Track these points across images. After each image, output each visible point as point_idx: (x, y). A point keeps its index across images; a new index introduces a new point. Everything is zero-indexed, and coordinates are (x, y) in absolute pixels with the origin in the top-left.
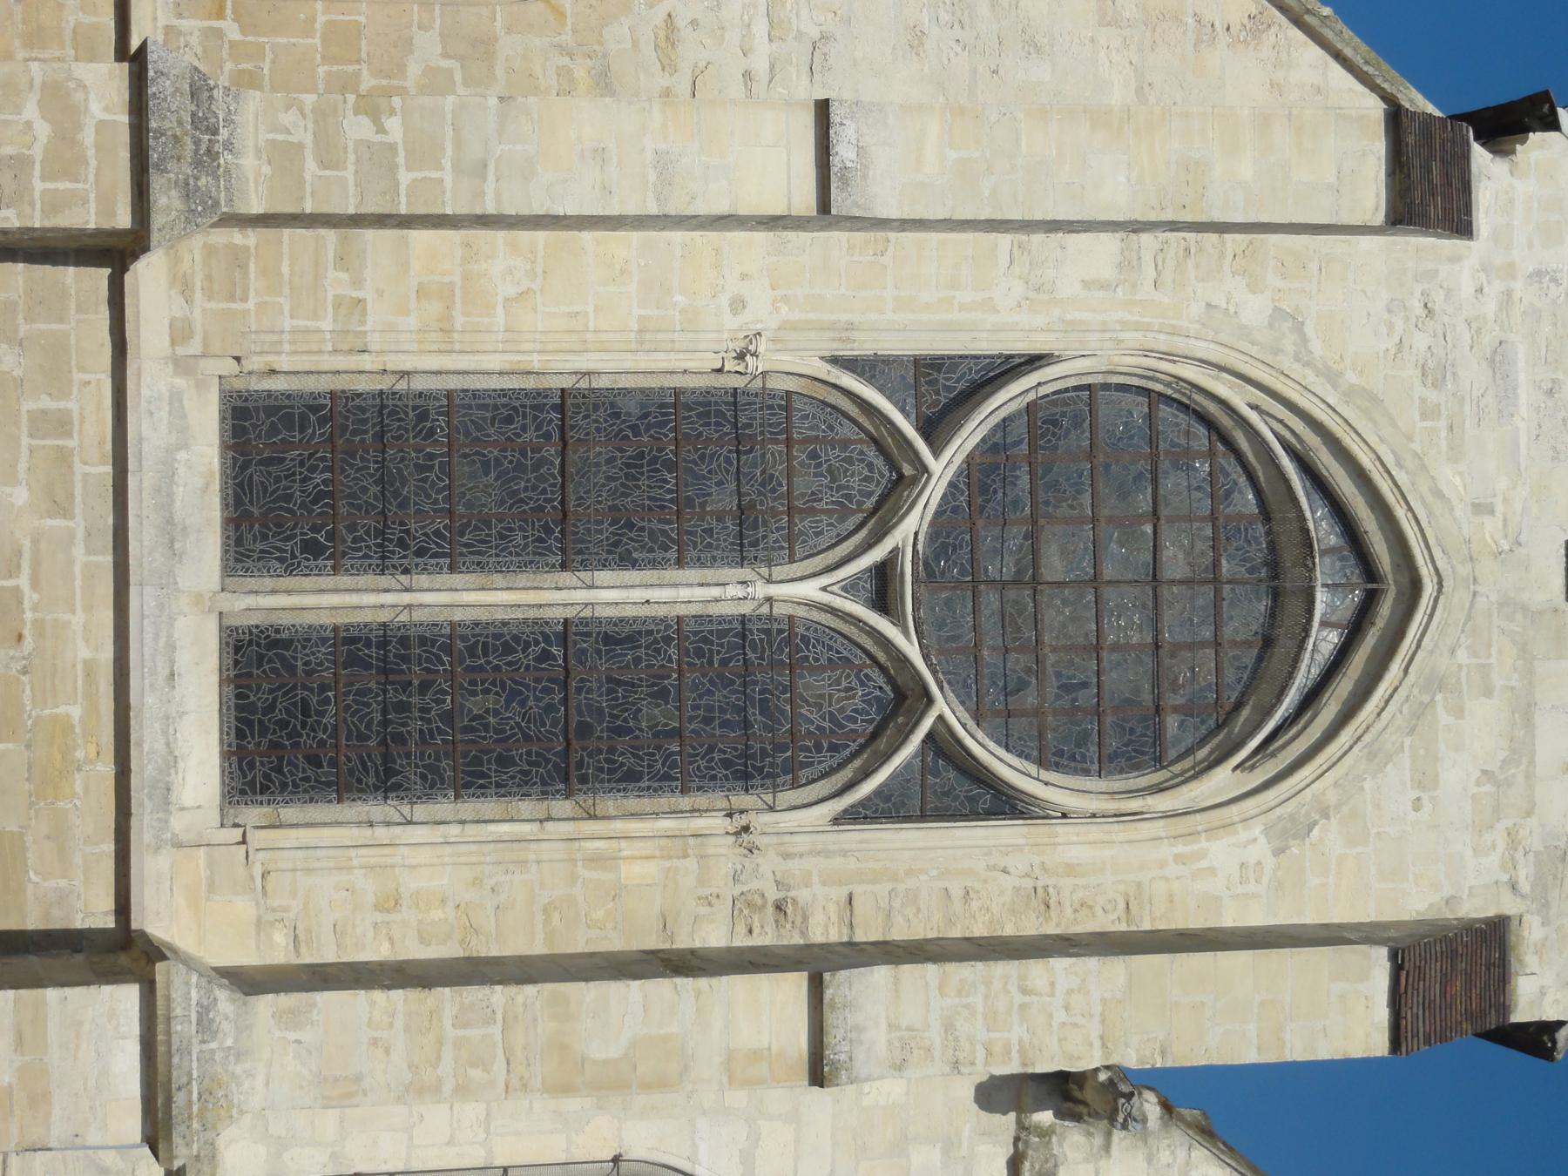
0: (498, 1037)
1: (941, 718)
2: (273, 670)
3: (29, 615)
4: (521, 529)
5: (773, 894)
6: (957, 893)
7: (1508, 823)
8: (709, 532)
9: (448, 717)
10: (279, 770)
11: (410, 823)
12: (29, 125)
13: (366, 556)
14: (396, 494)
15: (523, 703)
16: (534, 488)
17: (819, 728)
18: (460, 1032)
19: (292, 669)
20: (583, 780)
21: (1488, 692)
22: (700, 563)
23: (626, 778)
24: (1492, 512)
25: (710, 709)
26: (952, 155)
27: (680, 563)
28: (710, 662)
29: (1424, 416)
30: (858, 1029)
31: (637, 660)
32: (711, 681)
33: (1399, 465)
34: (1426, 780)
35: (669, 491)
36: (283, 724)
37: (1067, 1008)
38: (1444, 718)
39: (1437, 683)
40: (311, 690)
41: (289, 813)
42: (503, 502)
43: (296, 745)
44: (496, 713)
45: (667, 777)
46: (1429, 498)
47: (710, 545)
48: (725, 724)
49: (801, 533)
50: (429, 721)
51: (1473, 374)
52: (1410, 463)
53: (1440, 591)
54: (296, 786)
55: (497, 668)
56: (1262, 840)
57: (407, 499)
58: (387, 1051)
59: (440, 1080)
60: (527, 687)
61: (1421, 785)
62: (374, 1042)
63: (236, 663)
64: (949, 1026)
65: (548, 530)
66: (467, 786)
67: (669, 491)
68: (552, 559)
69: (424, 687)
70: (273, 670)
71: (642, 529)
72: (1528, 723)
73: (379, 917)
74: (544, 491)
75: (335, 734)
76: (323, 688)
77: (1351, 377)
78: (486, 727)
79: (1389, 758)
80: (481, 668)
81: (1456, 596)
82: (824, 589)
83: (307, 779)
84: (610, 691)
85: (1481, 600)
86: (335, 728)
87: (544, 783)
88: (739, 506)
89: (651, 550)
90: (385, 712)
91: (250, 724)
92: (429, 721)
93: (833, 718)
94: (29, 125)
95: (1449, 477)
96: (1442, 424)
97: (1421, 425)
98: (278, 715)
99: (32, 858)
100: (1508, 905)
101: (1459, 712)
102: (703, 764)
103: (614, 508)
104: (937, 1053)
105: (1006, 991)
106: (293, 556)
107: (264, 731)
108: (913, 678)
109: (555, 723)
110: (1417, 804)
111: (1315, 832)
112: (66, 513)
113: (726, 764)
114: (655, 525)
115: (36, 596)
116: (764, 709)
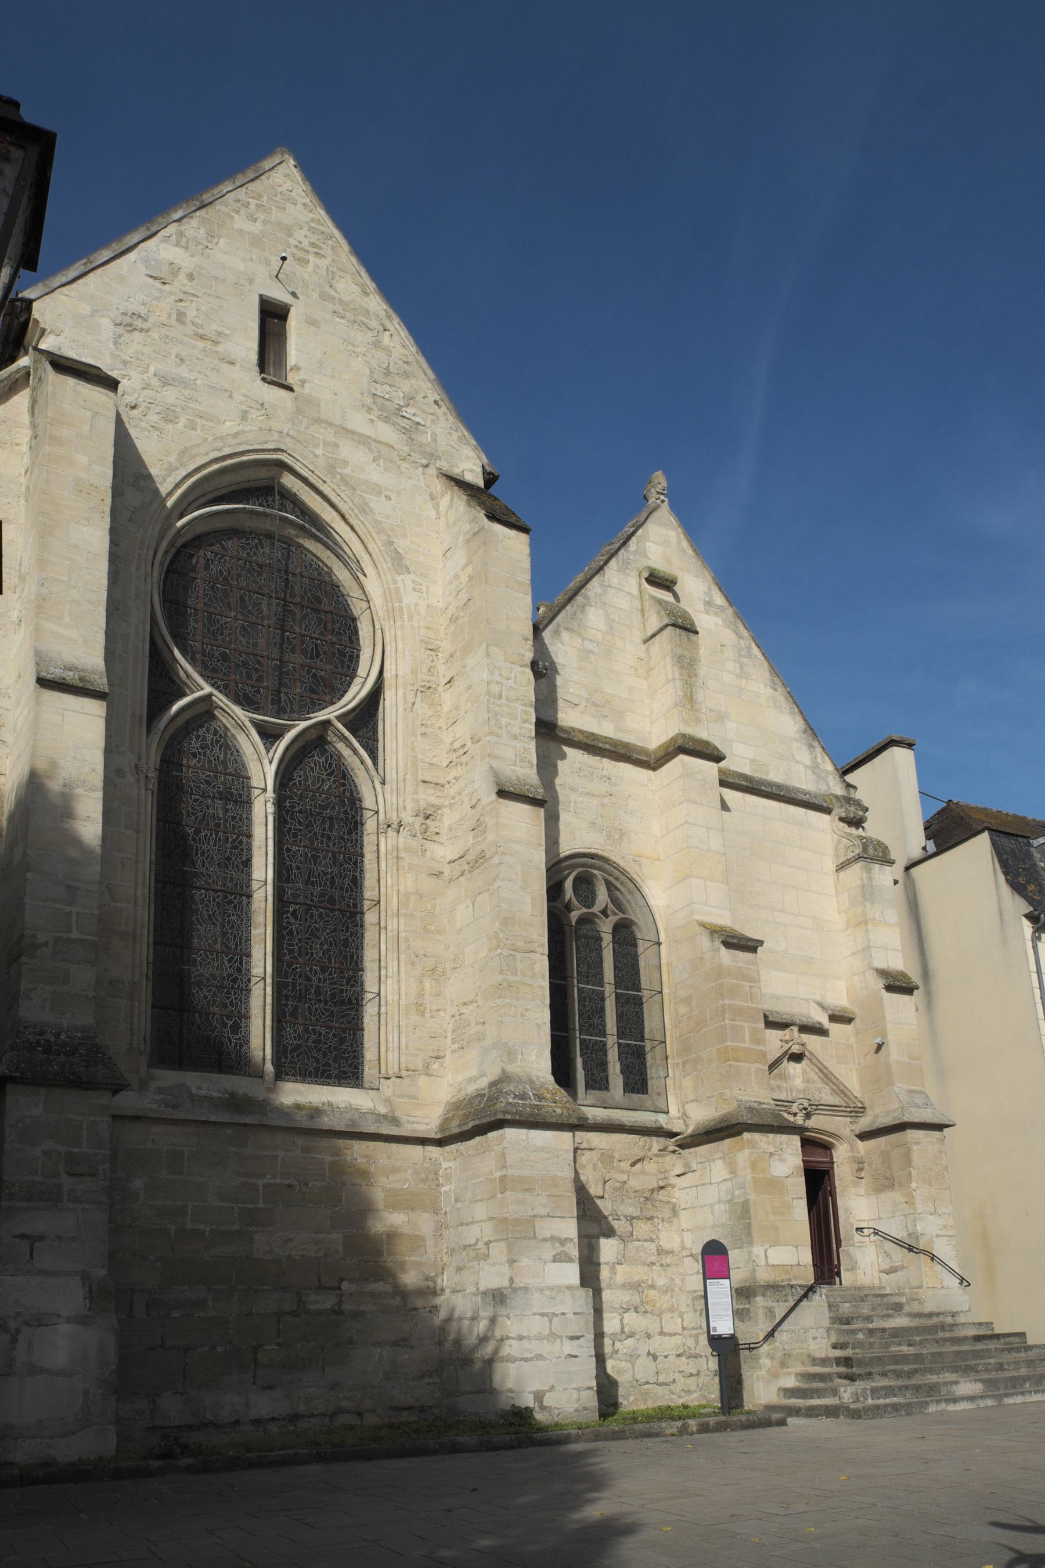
0: (521, 955)
1: (337, 718)
2: (298, 1056)
3: (278, 1181)
4: (229, 916)
5: (421, 819)
6: (423, 730)
7: (397, 459)
8: (233, 818)
9: (324, 970)
10: (347, 1059)
11: (379, 994)
12: (44, 1153)
13: (241, 1000)
14: (208, 980)
15: (318, 930)
16: (207, 906)
17: (334, 782)
18: (519, 973)
19: (298, 1046)
20: (355, 906)
21: (337, 446)
22: (249, 825)
23: (356, 883)
24: (246, 412)
25: (323, 835)
26: (67, 620)
27: (249, 836)
28: (300, 830)
29: (194, 429)
30: (518, 779)
31: (298, 868)
32: (310, 832)
33: (220, 450)
34: (377, 490)
35: (211, 834)
36: (325, 1054)
37: (508, 679)
38: (347, 471)
39: (331, 468)
40: (308, 1038)
41: (369, 1054)
42: (214, 924)
43: (335, 1049)
44: (322, 944)
45: (355, 863)
46: (237, 441)
47: (240, 819)
48: (331, 828)
49: (235, 770)
50: (325, 980)
51: (170, 395)
52: (219, 444)
53: (283, 451)
54: (355, 1051)
55: (300, 940)
56: (402, 577)
57: (211, 974)
58: (527, 1010)
59: (539, 986)
60: (309, 926)
61: (379, 493)
62: (523, 1015)
63: (293, 1075)
64: (515, 737)
65: (230, 902)
66: (357, 963)
67: (211, 834)
68: (245, 902)
69: (308, 979)
70: (298, 1056)
71: (231, 853)
72: (348, 431)
73: (428, 1015)
74: (209, 901)
75: (331, 1028)
76: (307, 1031)
77: (172, 459)
78: (329, 950)
79: (366, 504)
80: (300, 948)
81: (287, 444)
82: (271, 762)
83: (352, 1045)
84: (313, 884)
85: (291, 432)
86: (327, 1028)
87: (357, 926)
88: (220, 799)
89: (242, 850)
90: (320, 1001)
91: (324, 1071)
92: (325, 980)
93: (330, 774)
94: (44, 1153)
95: (230, 427)
96: (198, 420)
97: (199, 432)
98: (320, 1057)
99: (397, 1186)
100: (432, 471)
101: (346, 463)
102: (349, 844)
103: (219, 865)
104: (527, 746)
105: (499, 705)
106: (239, 1039)
107: (328, 1064)
108: (312, 731)
109: (327, 915)
110: (388, 498)
111: (400, 551)
112: (233, 1208)
113: (350, 833)
114: (229, 845)
115: (268, 1176)
116: (325, 808)
